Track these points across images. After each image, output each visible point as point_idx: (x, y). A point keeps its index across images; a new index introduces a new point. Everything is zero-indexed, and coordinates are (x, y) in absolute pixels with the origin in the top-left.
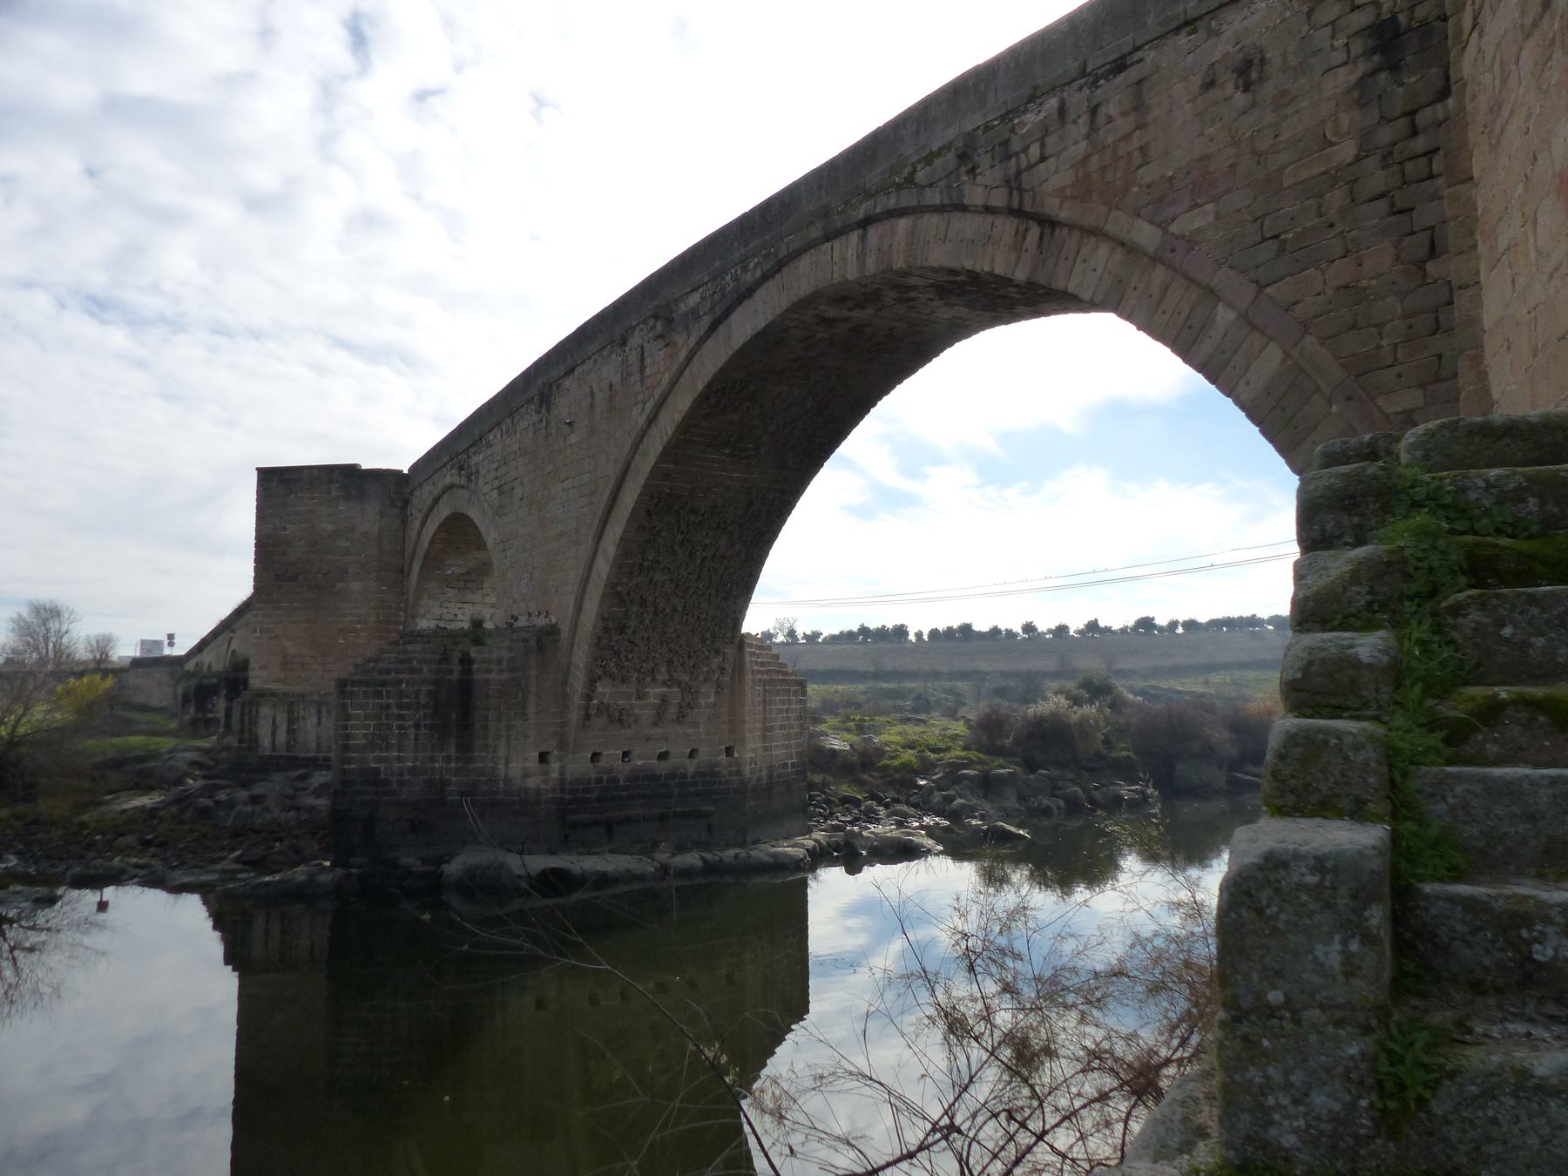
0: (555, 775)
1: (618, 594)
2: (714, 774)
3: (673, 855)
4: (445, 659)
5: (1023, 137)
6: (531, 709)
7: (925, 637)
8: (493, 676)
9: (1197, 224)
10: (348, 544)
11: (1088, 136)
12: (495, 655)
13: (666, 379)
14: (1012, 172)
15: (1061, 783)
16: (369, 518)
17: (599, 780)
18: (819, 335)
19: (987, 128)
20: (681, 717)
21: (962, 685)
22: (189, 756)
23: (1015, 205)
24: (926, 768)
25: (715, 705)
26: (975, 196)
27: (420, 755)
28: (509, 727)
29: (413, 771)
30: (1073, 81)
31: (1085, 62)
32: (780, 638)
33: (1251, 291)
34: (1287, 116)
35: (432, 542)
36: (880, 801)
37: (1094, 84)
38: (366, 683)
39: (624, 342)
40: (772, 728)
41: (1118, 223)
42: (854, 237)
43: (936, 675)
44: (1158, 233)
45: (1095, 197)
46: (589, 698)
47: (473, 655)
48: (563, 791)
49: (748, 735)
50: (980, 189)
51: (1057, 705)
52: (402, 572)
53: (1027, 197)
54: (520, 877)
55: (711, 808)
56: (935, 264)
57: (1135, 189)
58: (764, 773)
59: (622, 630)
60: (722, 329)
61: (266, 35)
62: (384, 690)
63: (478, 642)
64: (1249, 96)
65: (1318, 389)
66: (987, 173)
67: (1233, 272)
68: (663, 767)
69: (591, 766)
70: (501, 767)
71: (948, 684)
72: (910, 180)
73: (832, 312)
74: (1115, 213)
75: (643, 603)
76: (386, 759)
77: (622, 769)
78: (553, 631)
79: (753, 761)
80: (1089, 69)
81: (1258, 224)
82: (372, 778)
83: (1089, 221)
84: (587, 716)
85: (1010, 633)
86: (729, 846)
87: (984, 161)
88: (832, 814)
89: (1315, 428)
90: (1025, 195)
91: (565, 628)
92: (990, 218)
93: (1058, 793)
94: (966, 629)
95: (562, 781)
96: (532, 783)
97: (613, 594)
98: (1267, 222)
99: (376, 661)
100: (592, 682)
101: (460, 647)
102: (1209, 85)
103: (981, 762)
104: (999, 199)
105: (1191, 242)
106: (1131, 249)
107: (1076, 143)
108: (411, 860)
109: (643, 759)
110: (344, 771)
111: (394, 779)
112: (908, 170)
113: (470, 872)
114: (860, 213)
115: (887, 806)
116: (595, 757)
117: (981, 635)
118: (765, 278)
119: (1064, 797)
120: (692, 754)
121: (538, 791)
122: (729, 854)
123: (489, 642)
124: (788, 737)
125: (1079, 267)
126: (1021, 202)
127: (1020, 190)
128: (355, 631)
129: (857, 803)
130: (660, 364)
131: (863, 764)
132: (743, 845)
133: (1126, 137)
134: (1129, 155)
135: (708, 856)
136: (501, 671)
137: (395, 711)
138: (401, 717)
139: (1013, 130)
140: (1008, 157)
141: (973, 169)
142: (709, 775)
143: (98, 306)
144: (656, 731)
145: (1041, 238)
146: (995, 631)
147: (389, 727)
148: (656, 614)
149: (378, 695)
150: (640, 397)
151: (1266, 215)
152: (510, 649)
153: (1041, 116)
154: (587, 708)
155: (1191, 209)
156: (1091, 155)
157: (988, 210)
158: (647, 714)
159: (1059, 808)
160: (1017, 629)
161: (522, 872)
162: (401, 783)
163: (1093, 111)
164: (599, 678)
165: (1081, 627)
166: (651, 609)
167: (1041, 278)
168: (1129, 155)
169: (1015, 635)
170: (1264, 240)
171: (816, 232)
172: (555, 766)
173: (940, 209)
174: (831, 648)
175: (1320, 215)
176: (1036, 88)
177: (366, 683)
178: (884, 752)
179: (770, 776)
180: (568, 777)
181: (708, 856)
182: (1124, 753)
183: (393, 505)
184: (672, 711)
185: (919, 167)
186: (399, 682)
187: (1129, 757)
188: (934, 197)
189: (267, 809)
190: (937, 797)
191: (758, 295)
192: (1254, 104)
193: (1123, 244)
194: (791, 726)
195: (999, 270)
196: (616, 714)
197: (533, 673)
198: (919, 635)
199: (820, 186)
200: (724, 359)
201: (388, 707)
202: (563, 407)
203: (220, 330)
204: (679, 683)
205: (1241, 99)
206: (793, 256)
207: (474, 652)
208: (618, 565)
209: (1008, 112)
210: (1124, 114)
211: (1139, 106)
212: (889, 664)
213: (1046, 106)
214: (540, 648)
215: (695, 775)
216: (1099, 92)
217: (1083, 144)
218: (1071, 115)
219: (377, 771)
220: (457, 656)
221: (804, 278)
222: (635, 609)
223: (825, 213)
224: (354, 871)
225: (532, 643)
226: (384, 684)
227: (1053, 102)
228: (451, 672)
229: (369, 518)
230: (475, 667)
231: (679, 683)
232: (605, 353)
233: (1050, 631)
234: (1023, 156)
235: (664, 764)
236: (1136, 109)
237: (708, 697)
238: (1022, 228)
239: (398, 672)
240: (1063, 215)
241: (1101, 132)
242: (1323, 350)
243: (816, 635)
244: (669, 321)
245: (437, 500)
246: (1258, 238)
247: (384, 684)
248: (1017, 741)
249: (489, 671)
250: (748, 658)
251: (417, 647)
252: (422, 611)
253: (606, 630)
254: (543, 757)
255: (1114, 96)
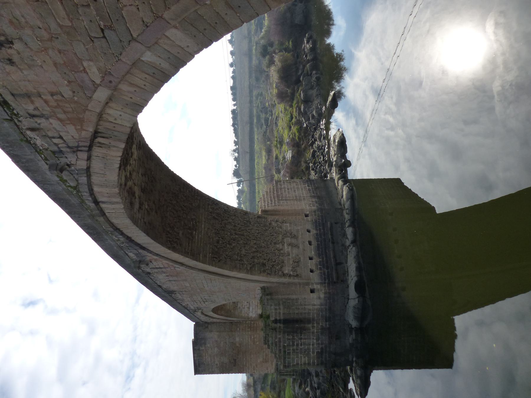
0: (319, 286)
1: (251, 268)
2: (316, 221)
3: (347, 238)
4: (275, 329)
5: (49, 145)
6: (294, 297)
7: (235, 103)
8: (282, 312)
9: (95, 70)
10: (222, 343)
11: (47, 119)
12: (273, 311)
13: (165, 262)
14: (68, 150)
15: (305, 72)
16: (212, 336)
17: (320, 269)
18: (146, 207)
19: (46, 159)
20: (295, 237)
21: (255, 93)
22: (297, 388)
23: (87, 149)
24: (299, 123)
25: (290, 223)
26: (82, 164)
27: (312, 337)
28: (301, 305)
29: (318, 339)
30: (16, 124)
31: (4, 119)
32: (236, 155)
33: (134, 44)
34: (26, 22)
35: (222, 315)
36: (313, 143)
37: (17, 115)
38: (285, 358)
39: (149, 273)
40: (296, 197)
41: (95, 106)
42: (103, 206)
43: (251, 102)
44: (100, 89)
45: (81, 116)
46: (290, 276)
47: (273, 319)
48: (325, 283)
49: (300, 208)
50: (78, 162)
51: (275, 71)
52: (231, 323)
53: (81, 144)
54: (359, 301)
55: (329, 223)
56: (117, 178)
57: (76, 98)
58: (314, 200)
59: (264, 265)
60: (144, 246)
61: (32, 333)
62: (287, 351)
63: (268, 317)
64: (15, 41)
65: (196, 11)
66: (69, 159)
67: (124, 53)
68: (314, 243)
69: (315, 272)
70: (316, 307)
71: (254, 98)
72: (75, 188)
73: (137, 206)
74: (90, 107)
75: (253, 257)
76: (313, 349)
77: (316, 260)
78: (263, 289)
79: (309, 206)
80: (9, 118)
81: (95, 40)
82: (320, 354)
83: (94, 119)
84: (297, 275)
85: (233, 72)
86: (342, 215)
87: (63, 161)
88: (320, 163)
89: (218, 13)
90: (80, 145)
91: (262, 285)
92: (93, 157)
93: (309, 73)
94: (232, 88)
95: (321, 283)
96: (322, 296)
97: (250, 271)
98: (93, 35)
99: (276, 354)
100: (284, 275)
101: (270, 323)
102: (11, 62)
103: (298, 102)
104: (84, 155)
105: (106, 73)
106: (110, 99)
107: (51, 124)
108: (351, 339)
109: (311, 251)
110: (318, 365)
111: (321, 346)
112: (69, 188)
113: (356, 318)
114: (92, 205)
115: (315, 140)
116: (312, 271)
117: (234, 83)
118: (122, 234)
119: (312, 70)
120: (309, 231)
121: (325, 293)
122: (347, 217)
123: (268, 313)
124: (298, 188)
125: (119, 122)
126: (85, 147)
127: (78, 146)
128: (254, 338)
129: (314, 152)
130: (160, 263)
131: (298, 147)
132: (342, 210)
133: (46, 102)
134: (56, 101)
135: (347, 225)
136: (280, 309)
137: (295, 347)
138: (297, 345)
139: (47, 149)
140: (61, 152)
141: (68, 165)
142: (317, 224)
143: (129, 378)
144: (301, 246)
145: (103, 137)
146: (233, 77)
147: (301, 349)
148: (257, 252)
149: (289, 353)
150: (173, 268)
151: (89, 36)
152: (271, 305)
153: (36, 137)
154: (294, 276)
155: (86, 72)
156: (57, 117)
157: (89, 159)
158: (295, 251)
159: (316, 74)
160: (232, 69)
161: (357, 300)
162: (322, 344)
163: (33, 116)
164: (283, 272)
165: (230, 46)
166: (256, 254)
167: (125, 138)
168: (56, 101)
169: (234, 70)
170: (104, 37)
171: (101, 219)
172: (315, 286)
173: (89, 176)
174: (240, 137)
175: (88, 6)
176: (22, 140)
177: (285, 358)
178: (293, 138)
179: (314, 197)
180: (320, 281)
181: (347, 225)
182: (290, 43)
183: (207, 327)
184: (294, 241)
185: (68, 184)
186: (284, 346)
187: (292, 41)
188: (83, 179)
189: (321, 372)
190: (312, 121)
191: (130, 235)
192: (20, 39)
193: (107, 103)
194: (294, 188)
195: (120, 154)
196: (296, 264)
197: (280, 297)
198: (234, 105)
199: (79, 217)
200: (158, 245)
201: (293, 350)
202: (173, 287)
203: (135, 340)
204: (283, 239)
205: (17, 45)
206: (112, 225)
207: (272, 319)
208: (240, 270)
209: (36, 151)
210: (32, 102)
211: (28, 96)
212: (246, 118)
213: (32, 136)
214: (270, 294)
215: (316, 230)
216: (21, 113)
217: (51, 120)
218: (37, 126)
219: (318, 352)
220: (274, 325)
221: (123, 221)
222: (256, 260)
223: (92, 216)
224: (354, 359)
225: (269, 297)
226: (285, 352)
227: (28, 133)
228: (280, 327)
229: (212, 336)
230: (278, 318)
231: (283, 239)
232: (153, 278)
233: (232, 57)
234: (60, 146)
235: (313, 243)
236: (29, 97)
237: (287, 227)
238: (98, 145)
239: (280, 346)
240: (91, 129)
241: (44, 113)
242: (173, 8)
243: (235, 142)
244: (140, 262)
245: (206, 315)
246: (104, 40)
247: (285, 352)
248: (288, 87)
249: (280, 313)
250: (270, 208)
251: (270, 339)
252: (246, 315)
253: (264, 271)
254: (312, 291)
255: (22, 107)
